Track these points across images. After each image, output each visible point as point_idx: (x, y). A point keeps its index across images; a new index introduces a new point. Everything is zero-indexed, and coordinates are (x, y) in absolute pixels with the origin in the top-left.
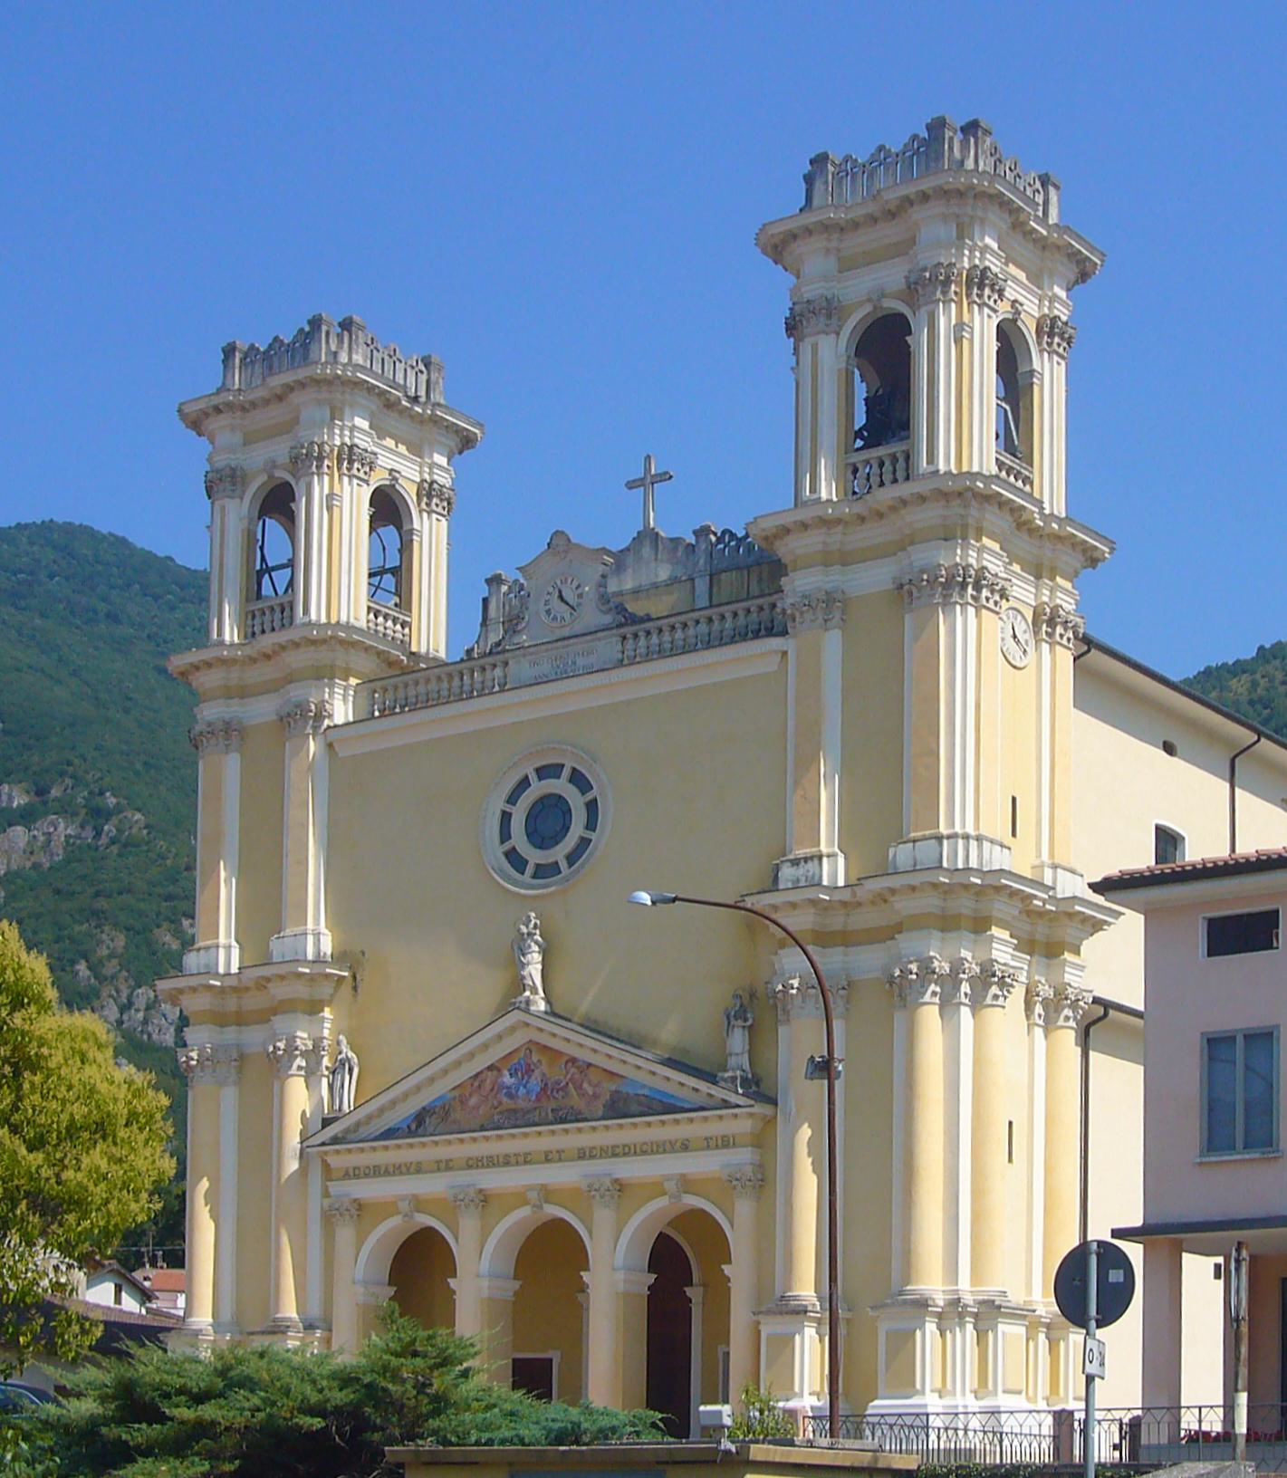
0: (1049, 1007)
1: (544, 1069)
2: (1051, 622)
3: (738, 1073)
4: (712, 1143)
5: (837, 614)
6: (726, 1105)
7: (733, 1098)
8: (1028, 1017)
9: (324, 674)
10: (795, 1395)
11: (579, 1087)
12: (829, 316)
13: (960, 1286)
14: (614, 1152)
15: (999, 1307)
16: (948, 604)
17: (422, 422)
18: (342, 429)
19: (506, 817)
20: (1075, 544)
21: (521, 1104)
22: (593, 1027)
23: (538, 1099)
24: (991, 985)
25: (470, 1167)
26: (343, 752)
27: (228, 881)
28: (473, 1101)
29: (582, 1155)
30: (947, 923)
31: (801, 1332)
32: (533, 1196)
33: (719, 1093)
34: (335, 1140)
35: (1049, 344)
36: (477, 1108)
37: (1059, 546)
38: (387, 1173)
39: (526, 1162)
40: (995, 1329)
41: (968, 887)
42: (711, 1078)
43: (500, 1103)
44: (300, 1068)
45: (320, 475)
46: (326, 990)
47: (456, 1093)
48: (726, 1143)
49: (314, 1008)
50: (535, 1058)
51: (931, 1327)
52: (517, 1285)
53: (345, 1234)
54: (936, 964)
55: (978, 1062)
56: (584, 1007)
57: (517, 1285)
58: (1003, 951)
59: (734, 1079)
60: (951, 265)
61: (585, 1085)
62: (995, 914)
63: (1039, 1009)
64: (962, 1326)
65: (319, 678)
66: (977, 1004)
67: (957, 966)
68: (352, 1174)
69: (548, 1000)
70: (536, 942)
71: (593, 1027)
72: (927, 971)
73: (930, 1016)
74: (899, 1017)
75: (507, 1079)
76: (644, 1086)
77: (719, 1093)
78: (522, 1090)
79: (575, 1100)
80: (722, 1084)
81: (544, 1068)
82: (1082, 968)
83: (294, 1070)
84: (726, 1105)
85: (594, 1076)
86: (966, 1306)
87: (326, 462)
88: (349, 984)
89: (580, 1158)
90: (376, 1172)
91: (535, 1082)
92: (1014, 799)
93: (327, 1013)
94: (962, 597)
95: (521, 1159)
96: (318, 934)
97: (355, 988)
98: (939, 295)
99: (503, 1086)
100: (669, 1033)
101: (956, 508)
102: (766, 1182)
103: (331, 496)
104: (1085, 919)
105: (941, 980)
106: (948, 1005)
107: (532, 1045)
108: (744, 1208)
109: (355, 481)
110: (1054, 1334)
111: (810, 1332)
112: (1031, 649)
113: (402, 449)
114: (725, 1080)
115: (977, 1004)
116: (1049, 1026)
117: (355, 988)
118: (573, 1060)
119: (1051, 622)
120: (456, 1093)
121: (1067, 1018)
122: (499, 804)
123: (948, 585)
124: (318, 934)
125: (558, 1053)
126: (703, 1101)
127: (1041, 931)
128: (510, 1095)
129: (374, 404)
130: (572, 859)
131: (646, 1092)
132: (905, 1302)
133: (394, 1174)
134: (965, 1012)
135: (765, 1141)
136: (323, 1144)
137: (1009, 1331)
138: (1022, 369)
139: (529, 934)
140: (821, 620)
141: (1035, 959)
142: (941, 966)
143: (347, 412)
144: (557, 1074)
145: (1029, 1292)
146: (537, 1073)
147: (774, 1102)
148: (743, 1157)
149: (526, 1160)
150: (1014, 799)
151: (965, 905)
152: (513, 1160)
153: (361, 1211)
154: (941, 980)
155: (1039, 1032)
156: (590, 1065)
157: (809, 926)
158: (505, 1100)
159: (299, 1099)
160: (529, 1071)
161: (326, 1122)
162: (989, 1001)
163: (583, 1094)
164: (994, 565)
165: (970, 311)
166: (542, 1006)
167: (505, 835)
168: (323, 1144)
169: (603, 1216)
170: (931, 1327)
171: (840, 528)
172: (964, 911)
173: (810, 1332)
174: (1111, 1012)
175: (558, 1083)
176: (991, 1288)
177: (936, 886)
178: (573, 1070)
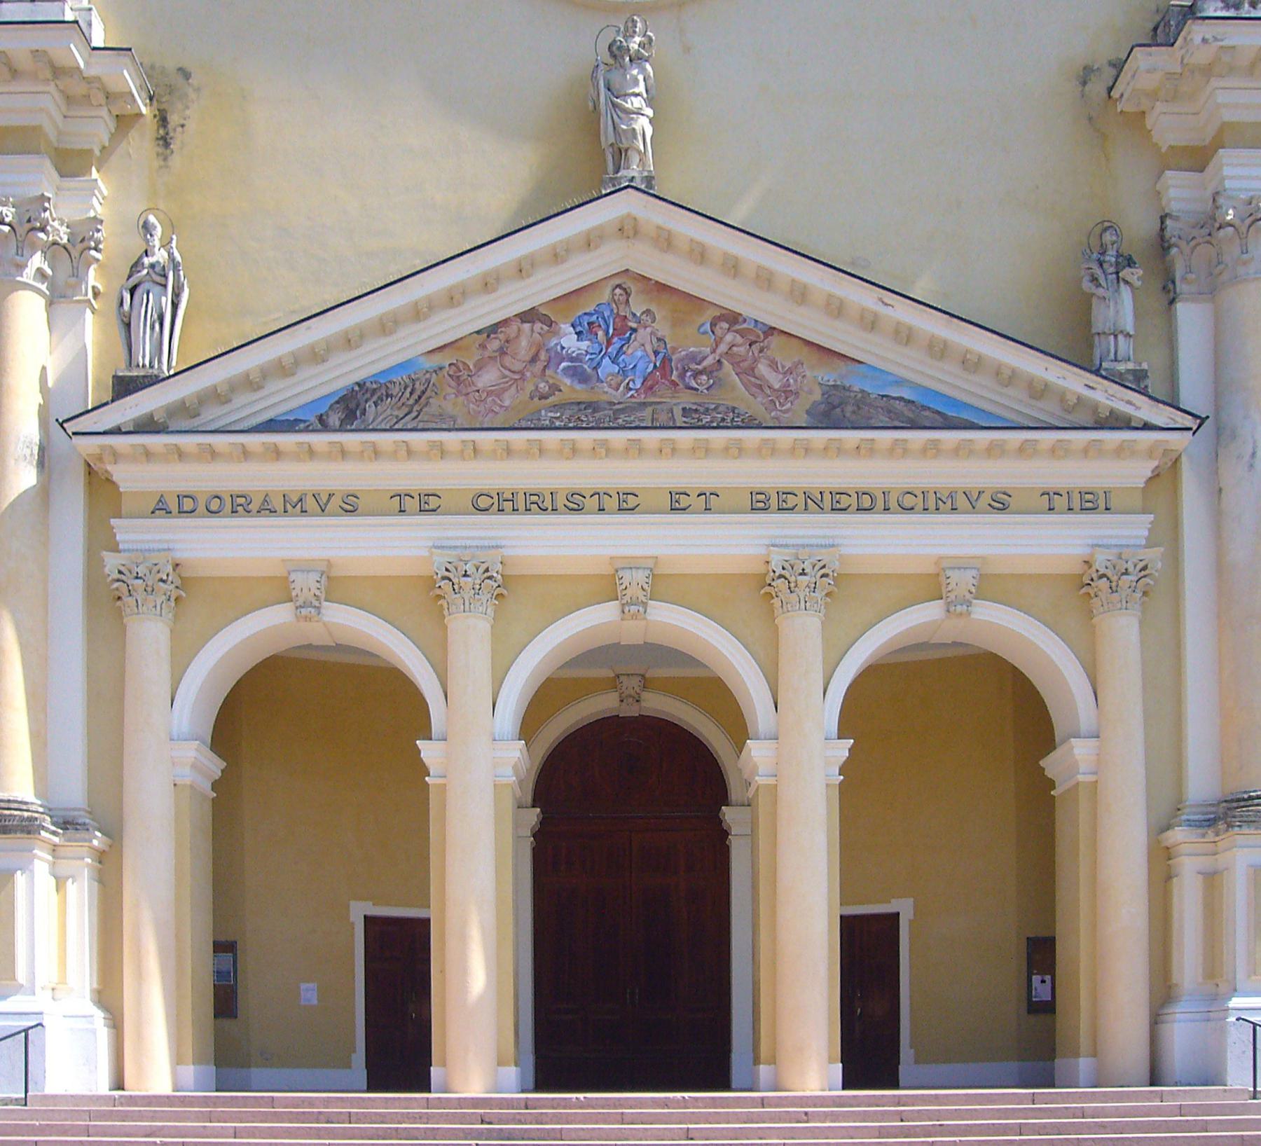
4: (1060, 502)
10: (19, 989)
14: (835, 502)
21: (606, 393)
23: (649, 388)
29: (760, 502)
31: (26, 867)
32: (306, 584)
34: (148, 426)
38: (266, 509)
43: (555, 388)
46: (95, 129)
47: (444, 360)
48: (1090, 502)
50: (638, 306)
53: (150, 634)
61: (763, 369)
75: (570, 341)
76: (900, 382)
79: (737, 393)
83: (28, 276)
91: (639, 352)
95: (561, 501)
97: (165, 141)
99: (559, 356)
107: (626, 282)
117: (165, 141)
118: (733, 318)
120: (437, 360)
125: (696, 303)
128: (583, 378)
136: (117, 431)
144: (691, 341)
146: (643, 335)
156: (771, 330)
160: (624, 330)
161: (124, 387)
163: (761, 386)
168: (117, 431)
169: (471, 631)
175: (693, 358)
177: (59, 72)
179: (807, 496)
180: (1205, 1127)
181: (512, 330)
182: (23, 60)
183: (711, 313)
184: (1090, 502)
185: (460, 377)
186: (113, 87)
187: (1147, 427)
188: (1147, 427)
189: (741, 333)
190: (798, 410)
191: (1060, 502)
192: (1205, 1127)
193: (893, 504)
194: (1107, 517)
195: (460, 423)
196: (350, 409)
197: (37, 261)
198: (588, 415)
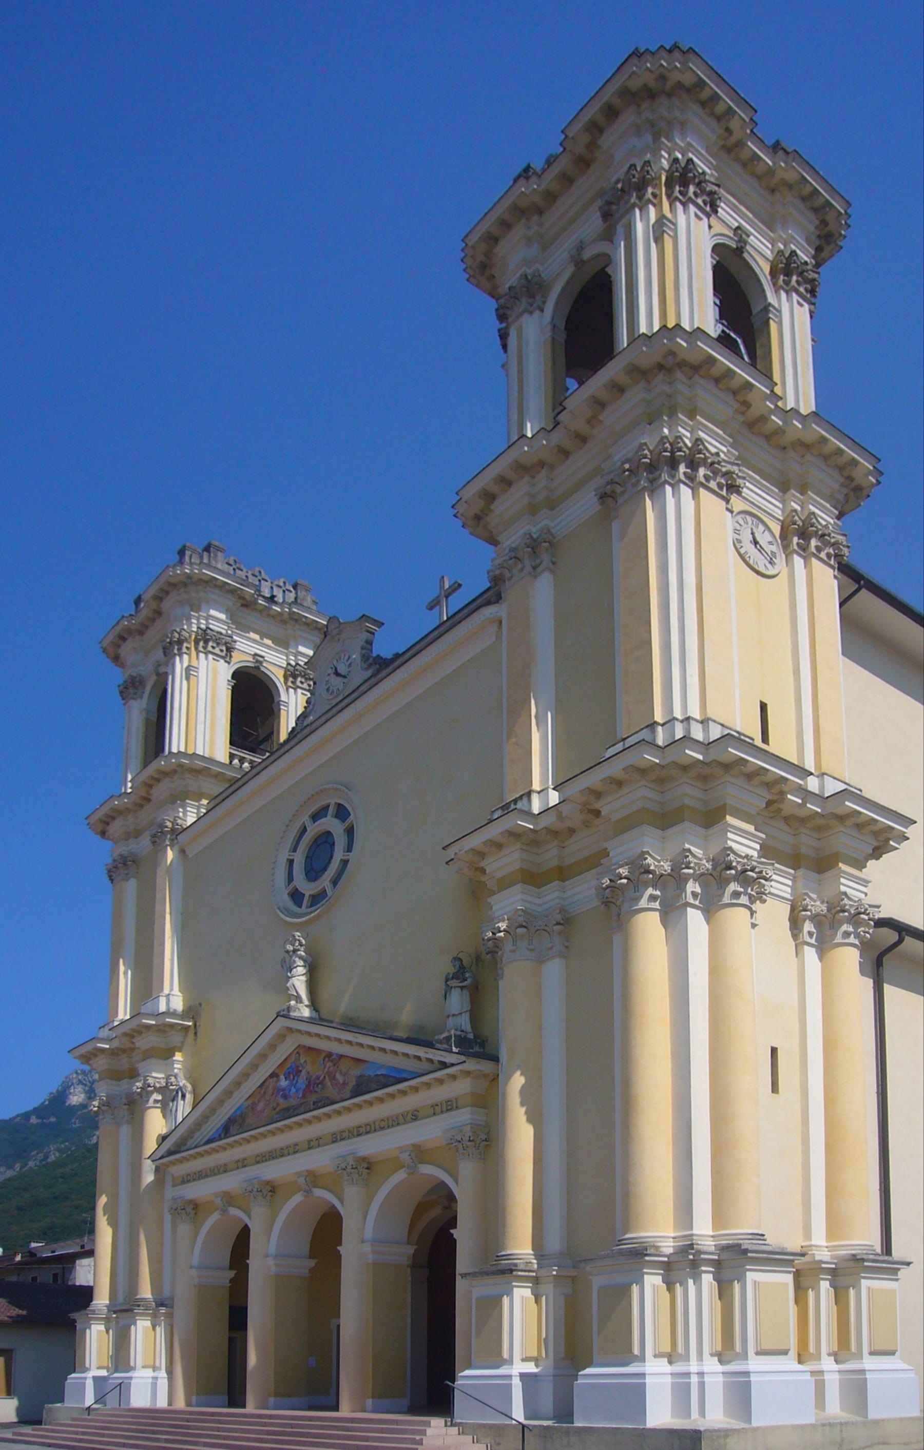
0: (820, 925)
1: (311, 1068)
2: (804, 534)
3: (453, 1032)
5: (546, 558)
6: (444, 1065)
7: (449, 1058)
8: (795, 936)
9: (179, 798)
11: (333, 1078)
12: (533, 296)
13: (695, 1231)
15: (746, 1251)
16: (655, 488)
17: (284, 622)
18: (198, 619)
19: (291, 862)
20: (831, 458)
21: (293, 1102)
22: (350, 1024)
24: (727, 881)
25: (258, 1162)
26: (190, 853)
27: (125, 973)
28: (260, 1107)
30: (666, 819)
31: (640, 1281)
33: (437, 1055)
35: (787, 283)
36: (262, 1111)
37: (808, 457)
39: (295, 1152)
40: (742, 1279)
41: (686, 768)
42: (429, 1044)
43: (278, 1104)
44: (156, 1101)
45: (180, 655)
46: (176, 1038)
47: (249, 1102)
48: (450, 1106)
49: (167, 1054)
51: (653, 1281)
52: (312, 1263)
54: (650, 860)
55: (716, 971)
56: (342, 1009)
57: (312, 1263)
58: (743, 842)
59: (448, 1038)
60: (648, 163)
61: (338, 1075)
62: (730, 802)
63: (808, 927)
64: (697, 1277)
65: (173, 802)
66: (710, 907)
67: (680, 861)
68: (187, 1179)
69: (314, 1005)
70: (301, 957)
71: (350, 1024)
72: (641, 874)
73: (648, 928)
74: (617, 938)
75: (284, 1083)
76: (382, 1066)
77: (437, 1055)
78: (293, 1090)
80: (438, 1046)
81: (309, 1067)
82: (865, 883)
84: (444, 1065)
85: (344, 1066)
86: (700, 1252)
87: (185, 645)
88: (192, 1031)
89: (333, 1142)
90: (201, 1175)
91: (302, 1082)
92: (763, 707)
93: (178, 1056)
94: (673, 477)
96: (172, 997)
97: (196, 1033)
98: (634, 199)
100: (406, 1015)
101: (660, 384)
102: (487, 1141)
103: (188, 669)
104: (864, 825)
105: (659, 880)
106: (672, 912)
108: (468, 1169)
109: (210, 656)
110: (842, 1281)
111: (522, 1294)
112: (780, 559)
113: (269, 642)
114: (441, 1042)
115: (710, 907)
116: (823, 947)
117: (196, 1033)
118: (329, 1055)
119: (804, 534)
121: (847, 934)
122: (284, 856)
123: (652, 467)
124: (172, 997)
125: (318, 1051)
126: (425, 1066)
127: (807, 842)
128: (285, 1097)
129: (230, 601)
130: (335, 882)
131: (383, 1072)
132: (621, 1253)
133: (211, 1176)
134: (695, 918)
135: (489, 1100)
137: (766, 1286)
138: (756, 308)
139: (295, 951)
140: (528, 568)
141: (800, 872)
142: (658, 863)
143: (204, 606)
145: (807, 1234)
146: (304, 1072)
147: (495, 1059)
148: (464, 1117)
149: (294, 1150)
150: (763, 707)
151: (687, 792)
152: (286, 1152)
153: (193, 1210)
154: (659, 880)
155: (810, 954)
156: (341, 1056)
157: (518, 866)
158: (281, 1101)
159: (156, 1124)
162: (726, 899)
164: (716, 445)
165: (672, 209)
166: (306, 1013)
167: (290, 878)
170: (653, 1281)
171: (544, 473)
172: (687, 801)
173: (522, 1294)
174: (908, 940)
176: (741, 1228)
177: (643, 772)
178: (329, 1064)
179: (349, 1131)
180: (367, 1439)
181: (267, 1084)
182: (621, 775)
183: (324, 1055)
184: (450, 1106)
185: (253, 1107)
186: (685, 762)
187: (453, 1065)
188: (453, 1065)
189: (332, 1061)
190: (347, 1092)
191: (438, 1109)
192: (367, 1439)
193: (377, 1127)
194: (458, 1111)
195: (254, 1126)
196: (226, 1130)
197: (692, 887)
198: (288, 1113)
